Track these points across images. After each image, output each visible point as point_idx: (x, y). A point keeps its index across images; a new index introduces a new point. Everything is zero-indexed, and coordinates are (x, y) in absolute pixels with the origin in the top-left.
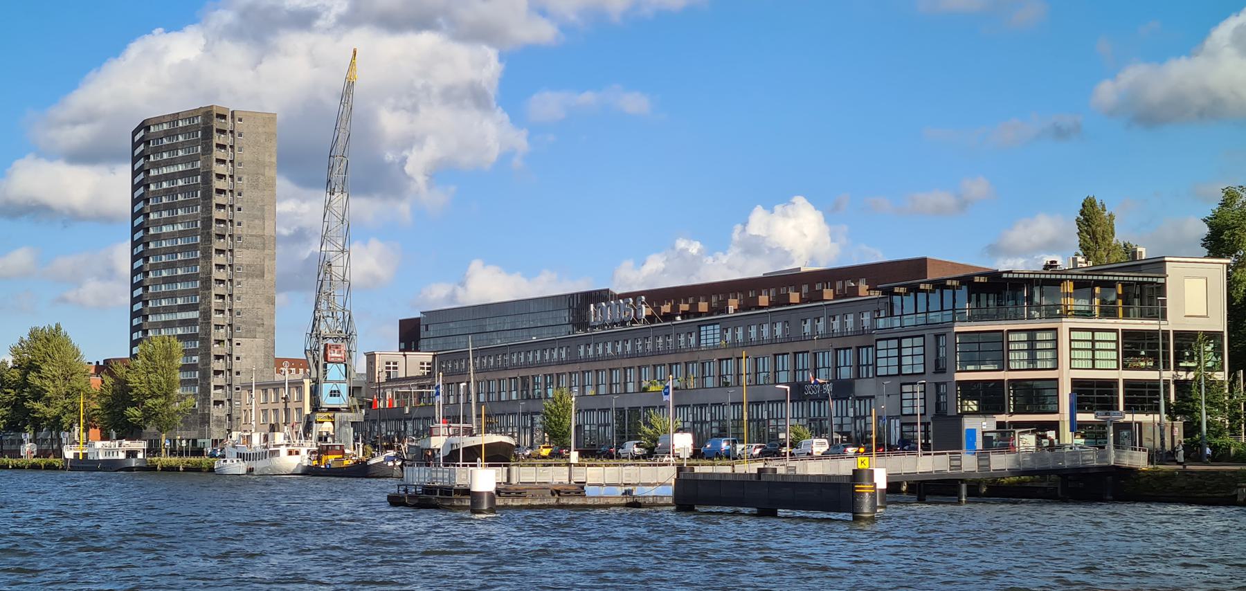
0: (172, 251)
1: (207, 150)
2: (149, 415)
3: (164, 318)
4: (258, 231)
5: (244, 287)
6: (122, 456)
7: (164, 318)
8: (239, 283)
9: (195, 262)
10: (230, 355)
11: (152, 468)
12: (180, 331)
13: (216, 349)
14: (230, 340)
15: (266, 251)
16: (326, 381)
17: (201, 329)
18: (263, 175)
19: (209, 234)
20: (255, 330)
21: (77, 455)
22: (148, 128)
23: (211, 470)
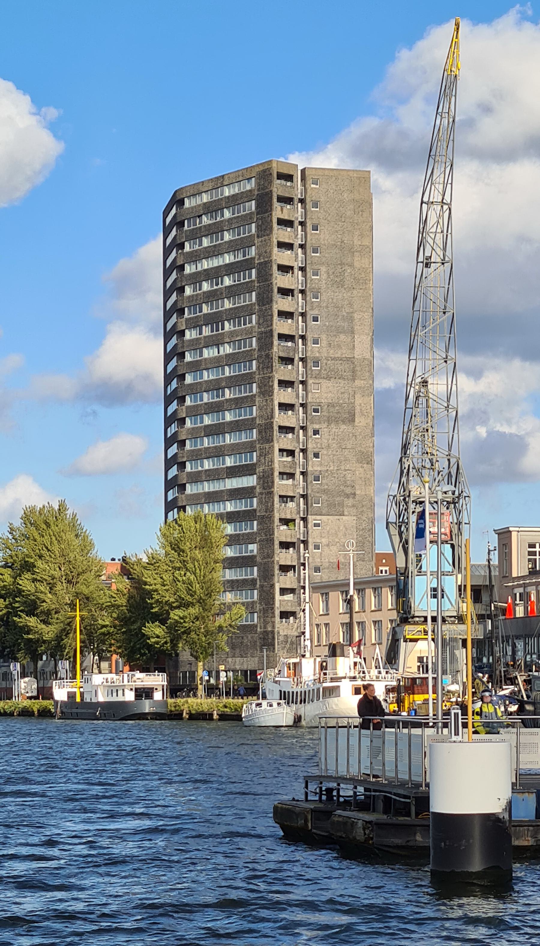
0: (216, 386)
1: (265, 229)
2: (176, 633)
3: (207, 487)
4: (345, 352)
5: (326, 439)
6: (130, 696)
7: (207, 487)
8: (316, 432)
9: (249, 401)
10: (305, 542)
11: (175, 716)
12: (230, 507)
13: (282, 533)
14: (304, 519)
15: (358, 383)
16: (420, 572)
17: (260, 502)
18: (351, 265)
19: (269, 357)
20: (341, 504)
21: (71, 696)
22: (181, 203)
23: (235, 717)
